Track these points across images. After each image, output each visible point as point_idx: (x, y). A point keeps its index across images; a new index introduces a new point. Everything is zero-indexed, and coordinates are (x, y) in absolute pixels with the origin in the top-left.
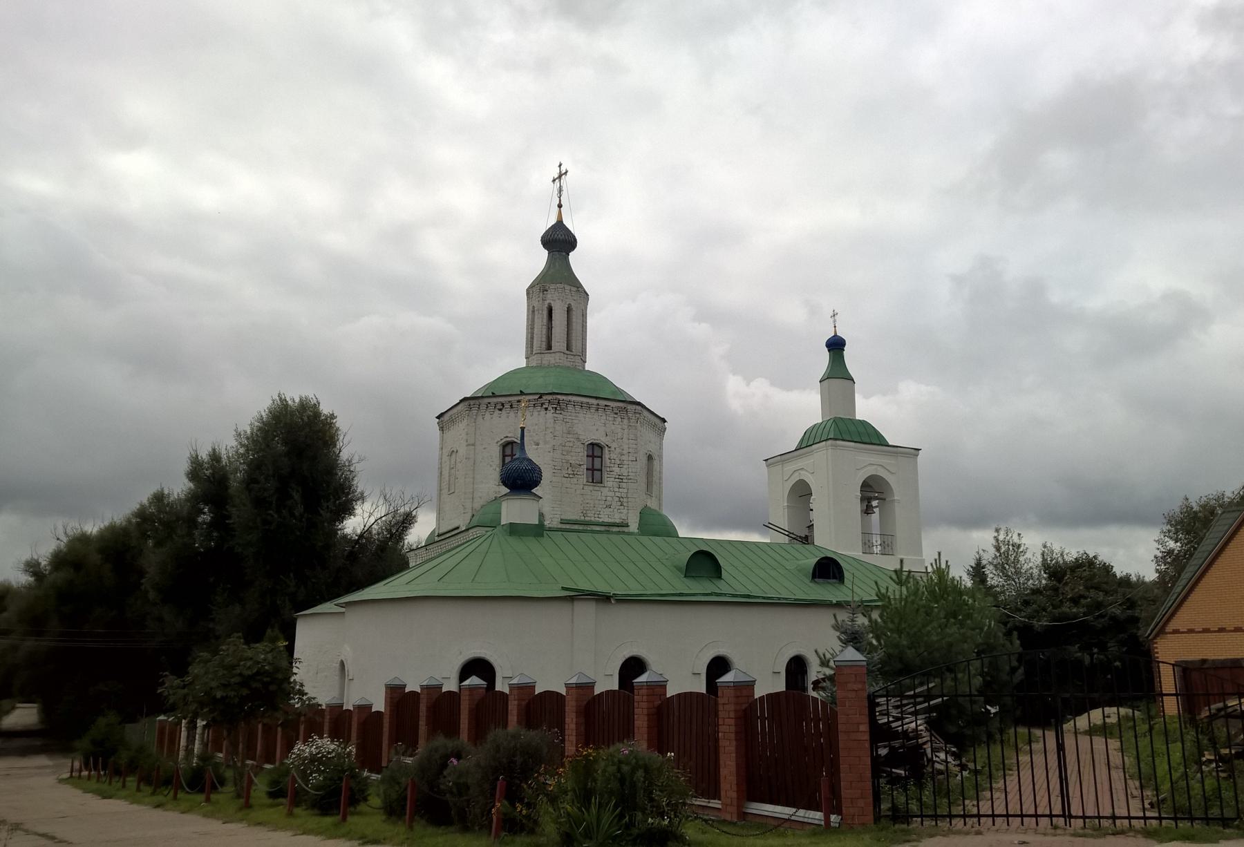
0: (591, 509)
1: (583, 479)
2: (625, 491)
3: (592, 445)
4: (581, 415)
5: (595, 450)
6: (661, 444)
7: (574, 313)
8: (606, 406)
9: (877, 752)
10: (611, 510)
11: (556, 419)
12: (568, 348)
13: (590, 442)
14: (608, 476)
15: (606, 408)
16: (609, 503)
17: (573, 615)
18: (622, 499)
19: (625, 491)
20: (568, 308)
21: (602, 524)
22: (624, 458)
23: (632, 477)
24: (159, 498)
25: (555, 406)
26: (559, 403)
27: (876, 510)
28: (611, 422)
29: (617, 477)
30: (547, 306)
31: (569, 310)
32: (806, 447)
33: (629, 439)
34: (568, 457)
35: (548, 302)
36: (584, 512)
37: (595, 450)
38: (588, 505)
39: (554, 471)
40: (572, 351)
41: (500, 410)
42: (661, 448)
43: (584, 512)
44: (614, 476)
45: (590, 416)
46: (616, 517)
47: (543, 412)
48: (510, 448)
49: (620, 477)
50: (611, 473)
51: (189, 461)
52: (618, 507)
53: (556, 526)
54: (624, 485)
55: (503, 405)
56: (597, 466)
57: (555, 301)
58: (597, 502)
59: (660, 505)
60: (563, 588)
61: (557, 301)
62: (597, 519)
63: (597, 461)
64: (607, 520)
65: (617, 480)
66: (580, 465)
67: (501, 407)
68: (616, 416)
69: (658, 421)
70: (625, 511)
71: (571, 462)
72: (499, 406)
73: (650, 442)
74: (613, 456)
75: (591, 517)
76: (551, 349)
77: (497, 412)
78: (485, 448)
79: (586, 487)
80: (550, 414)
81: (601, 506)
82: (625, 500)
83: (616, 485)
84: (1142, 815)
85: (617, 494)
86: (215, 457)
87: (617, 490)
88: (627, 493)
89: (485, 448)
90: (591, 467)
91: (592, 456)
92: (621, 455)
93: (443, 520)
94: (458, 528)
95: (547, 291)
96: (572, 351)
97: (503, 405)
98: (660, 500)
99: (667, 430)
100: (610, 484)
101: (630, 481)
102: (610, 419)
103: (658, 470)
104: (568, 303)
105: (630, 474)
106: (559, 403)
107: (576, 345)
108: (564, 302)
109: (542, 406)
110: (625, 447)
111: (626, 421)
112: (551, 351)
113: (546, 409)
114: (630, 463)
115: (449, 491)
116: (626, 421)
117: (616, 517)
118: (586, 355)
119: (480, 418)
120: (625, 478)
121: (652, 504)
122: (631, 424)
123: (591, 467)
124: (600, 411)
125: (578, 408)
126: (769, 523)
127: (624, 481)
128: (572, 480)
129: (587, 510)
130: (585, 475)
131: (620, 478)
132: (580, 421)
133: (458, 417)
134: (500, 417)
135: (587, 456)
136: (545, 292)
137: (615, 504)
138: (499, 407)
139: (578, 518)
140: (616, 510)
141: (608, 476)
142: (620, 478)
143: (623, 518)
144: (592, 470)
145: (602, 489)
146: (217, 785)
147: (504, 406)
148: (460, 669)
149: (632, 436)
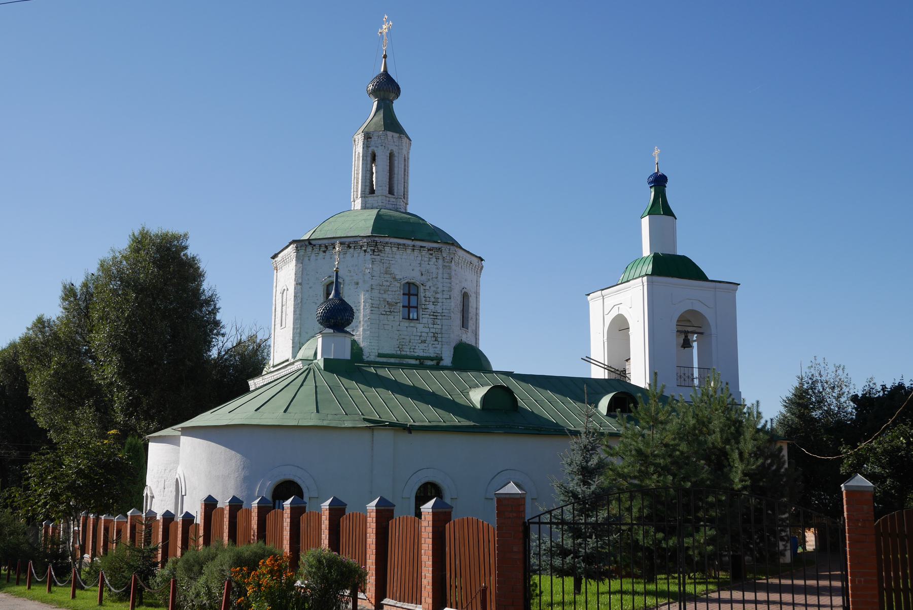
0: (407, 344)
1: (399, 317)
2: (439, 327)
3: (409, 284)
4: (398, 256)
5: (411, 290)
6: (478, 282)
7: (396, 158)
8: (421, 247)
9: (843, 584)
10: (426, 345)
11: (374, 260)
12: (391, 192)
13: (407, 281)
14: (424, 313)
15: (422, 249)
16: (423, 339)
17: (373, 437)
18: (436, 335)
19: (439, 327)
20: (390, 154)
21: (416, 358)
22: (439, 296)
23: (445, 314)
24: (41, 324)
25: (373, 248)
26: (376, 245)
27: (695, 344)
28: (427, 263)
29: (432, 313)
30: (370, 152)
31: (391, 156)
32: (633, 279)
33: (443, 278)
34: (385, 296)
35: (372, 148)
36: (401, 347)
37: (411, 290)
38: (404, 340)
39: (373, 309)
40: (394, 195)
41: (324, 252)
42: (478, 285)
43: (401, 347)
44: (428, 313)
45: (406, 257)
46: (430, 351)
47: (362, 254)
48: (334, 285)
49: (435, 314)
50: (426, 310)
51: (139, 231)
52: (432, 342)
53: (373, 360)
54: (439, 322)
55: (326, 247)
56: (413, 303)
57: (378, 147)
58: (412, 337)
59: (477, 339)
60: (365, 420)
61: (380, 147)
62: (413, 353)
63: (413, 299)
64: (421, 354)
65: (432, 317)
66: (397, 303)
67: (325, 249)
68: (431, 256)
69: (475, 260)
70: (439, 346)
71: (387, 300)
72: (323, 249)
73: (466, 280)
74: (428, 294)
75: (407, 351)
76: (374, 193)
77: (321, 254)
78: (310, 288)
79: (402, 324)
80: (368, 256)
81: (416, 341)
82: (439, 336)
83: (430, 321)
84: (766, 599)
85: (432, 330)
86: (83, 283)
87: (432, 326)
88: (442, 329)
89: (310, 288)
90: (407, 305)
91: (408, 294)
92: (436, 293)
93: (277, 352)
94: (288, 360)
95: (371, 138)
96: (394, 195)
97: (326, 247)
98: (476, 335)
99: (484, 269)
100: (425, 321)
101: (444, 318)
102: (426, 259)
103: (475, 306)
104: (390, 149)
105: (444, 311)
106: (376, 245)
107: (399, 188)
108: (387, 148)
109: (361, 248)
110: (440, 285)
111: (440, 261)
112: (375, 195)
113: (365, 251)
114: (444, 300)
115: (281, 326)
116: (440, 261)
117: (430, 351)
118: (407, 198)
119: (306, 259)
120: (439, 314)
121: (467, 338)
122: (445, 264)
123: (407, 305)
124: (416, 252)
125: (395, 249)
126: (586, 357)
127: (438, 317)
128: (389, 317)
129: (402, 345)
130: (401, 312)
131: (435, 315)
132: (396, 261)
133: (288, 258)
134: (324, 258)
135: (404, 294)
136: (369, 140)
137: (430, 340)
138: (324, 249)
139: (394, 352)
140: (430, 345)
141: (424, 313)
142: (435, 315)
143: (438, 352)
144: (408, 307)
145: (418, 325)
146: (84, 585)
147: (327, 248)
148: (274, 487)
149: (446, 276)
